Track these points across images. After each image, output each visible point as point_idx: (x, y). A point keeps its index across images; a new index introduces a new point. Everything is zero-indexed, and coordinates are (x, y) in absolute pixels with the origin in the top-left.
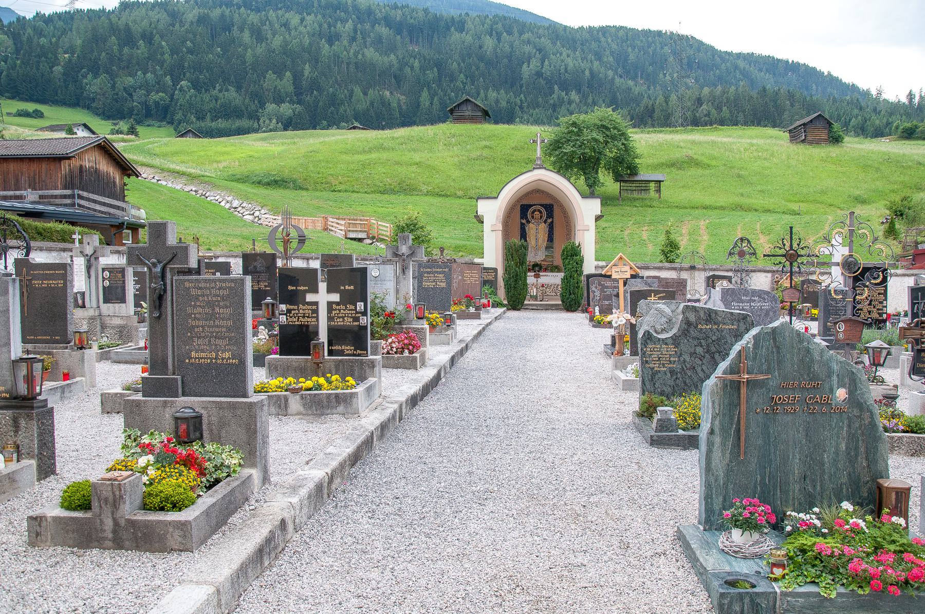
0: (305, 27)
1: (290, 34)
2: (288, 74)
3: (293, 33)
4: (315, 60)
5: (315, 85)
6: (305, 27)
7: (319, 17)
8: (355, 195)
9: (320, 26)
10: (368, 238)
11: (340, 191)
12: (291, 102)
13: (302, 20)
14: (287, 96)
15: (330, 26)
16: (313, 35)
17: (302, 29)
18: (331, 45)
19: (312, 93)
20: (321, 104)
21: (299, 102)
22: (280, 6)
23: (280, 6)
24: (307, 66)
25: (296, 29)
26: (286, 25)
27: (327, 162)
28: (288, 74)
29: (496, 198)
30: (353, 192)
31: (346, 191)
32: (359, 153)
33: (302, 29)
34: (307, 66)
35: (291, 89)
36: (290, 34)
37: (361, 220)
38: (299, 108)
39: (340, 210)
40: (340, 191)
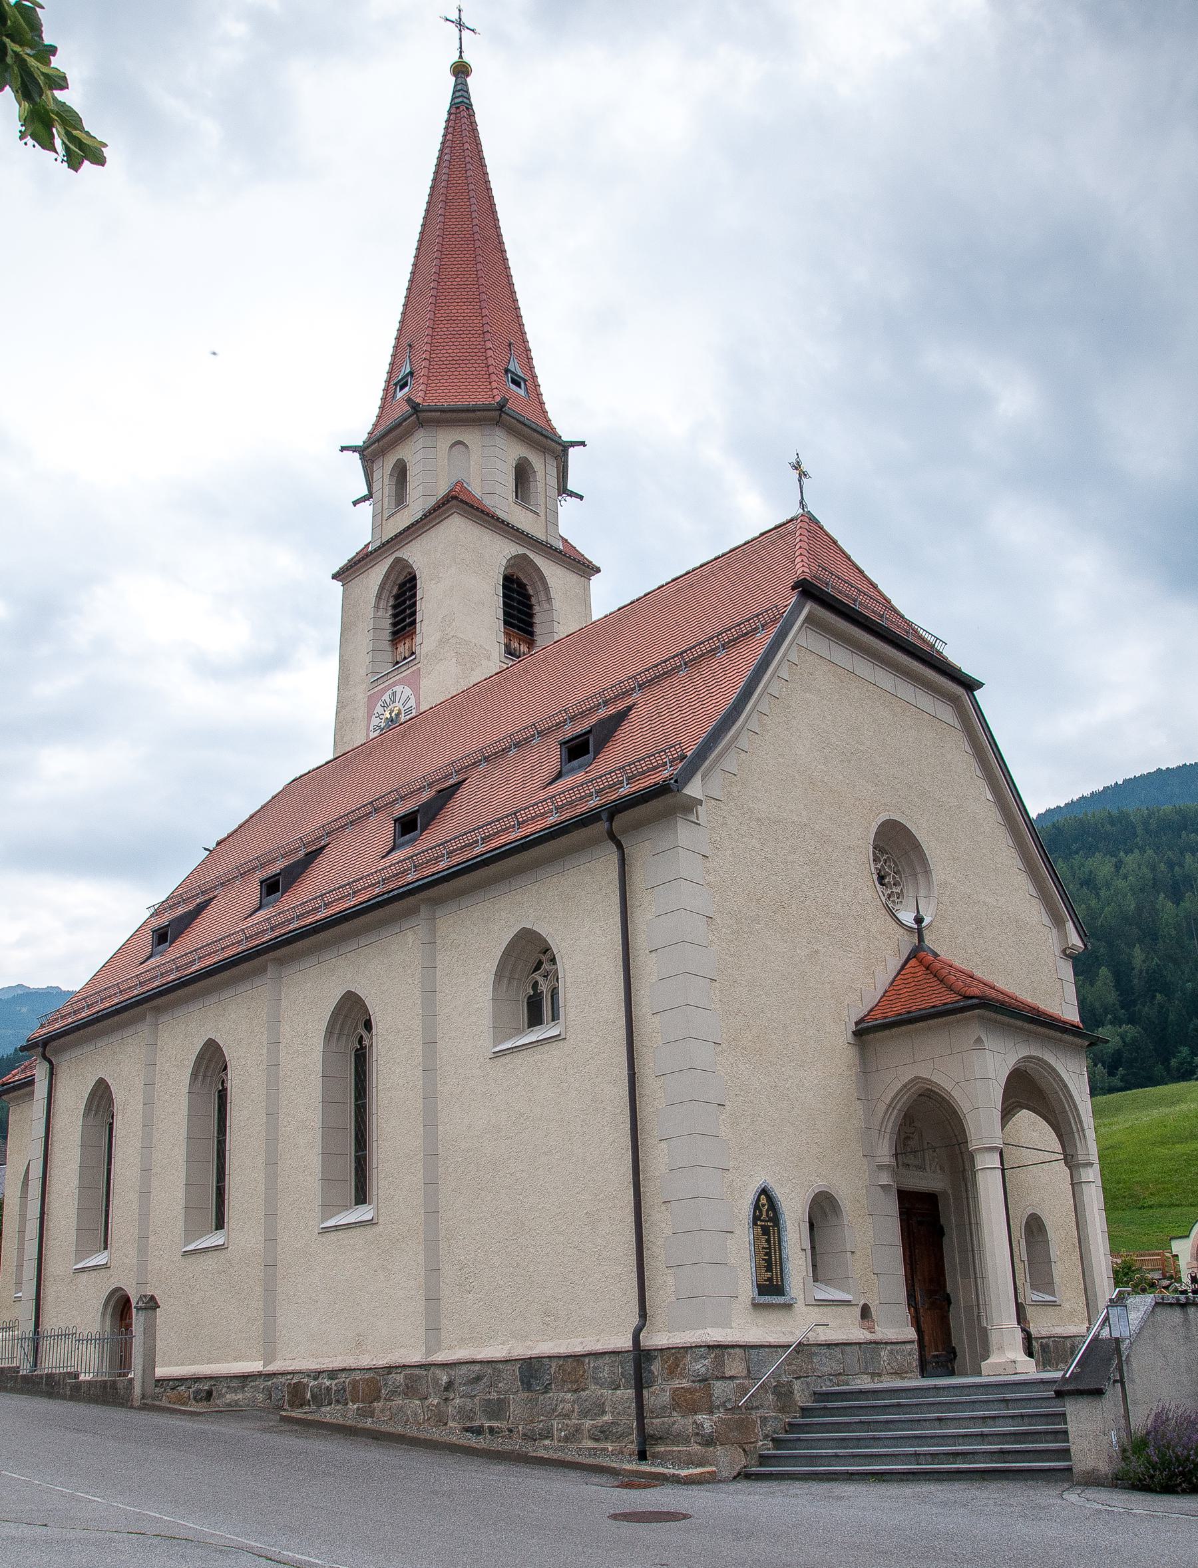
0: (1125, 877)
1: (1098, 896)
2: (1104, 971)
3: (1104, 893)
4: (1151, 936)
5: (1156, 983)
6: (1125, 877)
7: (1150, 852)
8: (1173, 1211)
9: (1153, 869)
10: (1164, 1278)
11: (1151, 1207)
12: (1117, 1021)
13: (1118, 866)
14: (1106, 1011)
15: (1171, 865)
16: (1142, 890)
17: (1120, 883)
18: (1177, 903)
19: (1154, 997)
20: (1172, 1017)
21: (1131, 1021)
22: (1074, 847)
23: (1074, 847)
24: (1137, 950)
25: (1108, 885)
26: (1089, 882)
27: (1132, 1162)
28: (1104, 971)
29: (1188, 1236)
30: (1172, 1205)
31: (1161, 1206)
32: (1182, 1140)
33: (1120, 883)
34: (1137, 950)
35: (1112, 997)
36: (1098, 896)
37: (1150, 1255)
38: (1130, 1030)
39: (1145, 1239)
40: (1151, 1207)
